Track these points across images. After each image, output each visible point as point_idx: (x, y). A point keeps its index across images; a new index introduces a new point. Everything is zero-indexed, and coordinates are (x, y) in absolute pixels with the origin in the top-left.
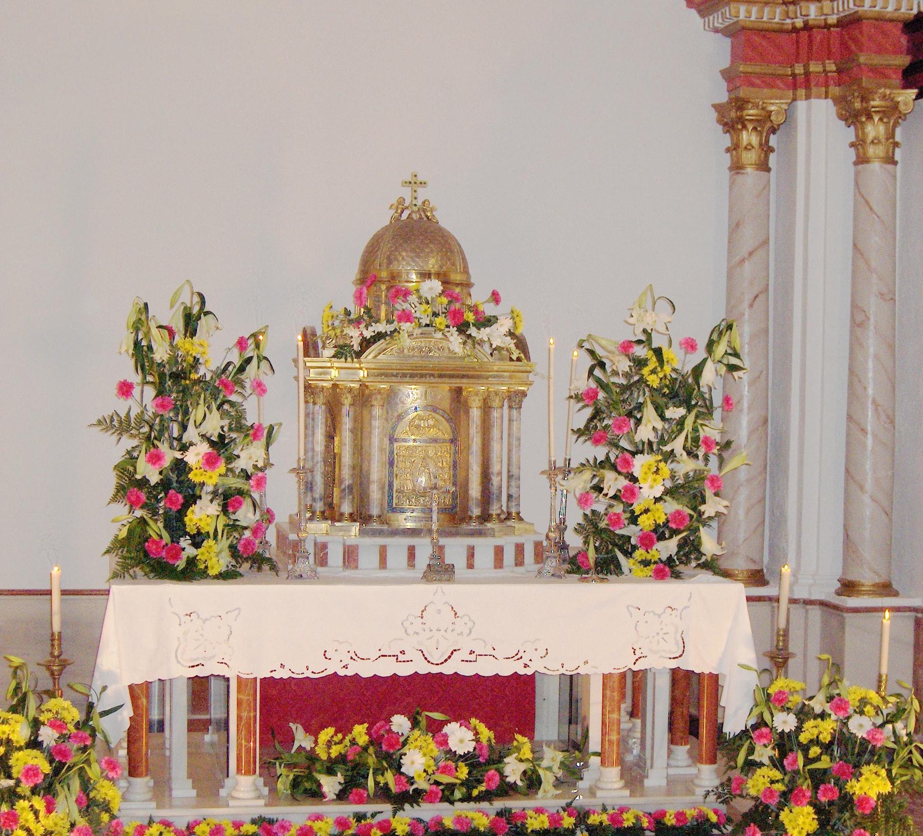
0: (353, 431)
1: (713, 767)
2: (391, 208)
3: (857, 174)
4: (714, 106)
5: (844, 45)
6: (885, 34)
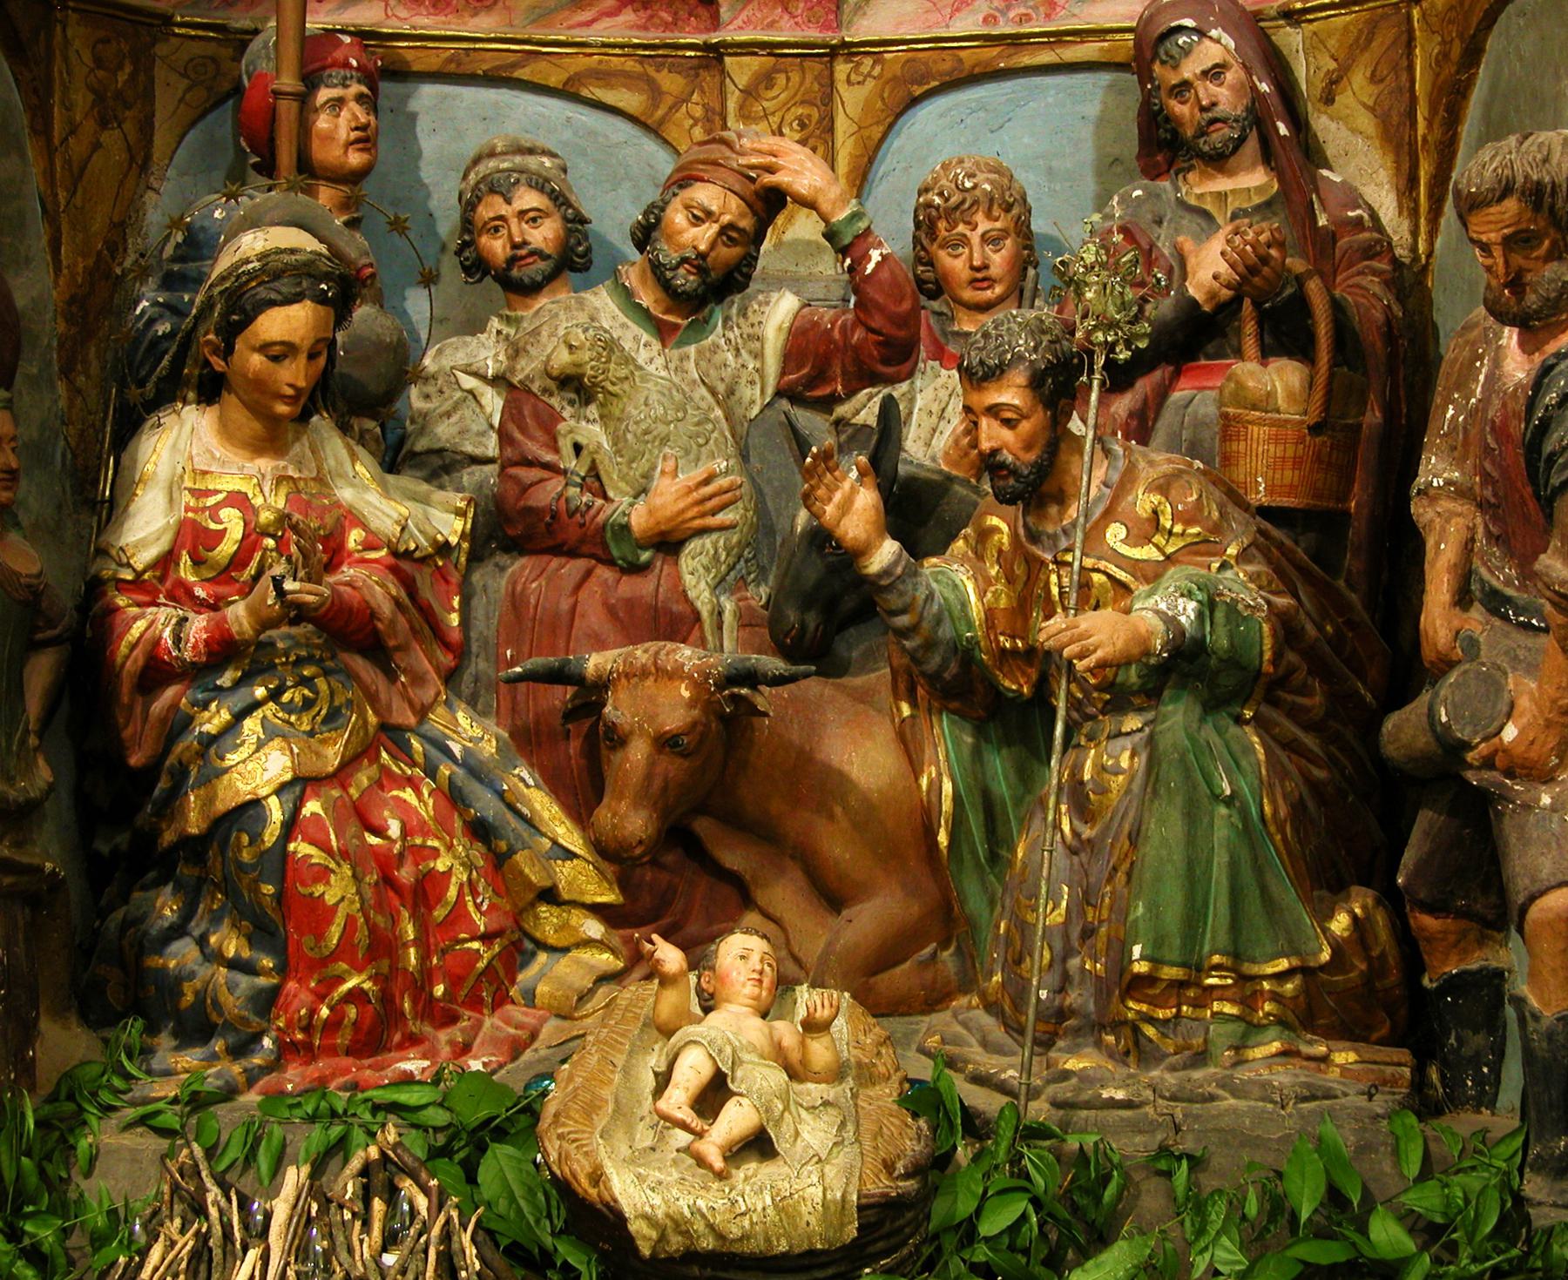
2: (92, 1160)
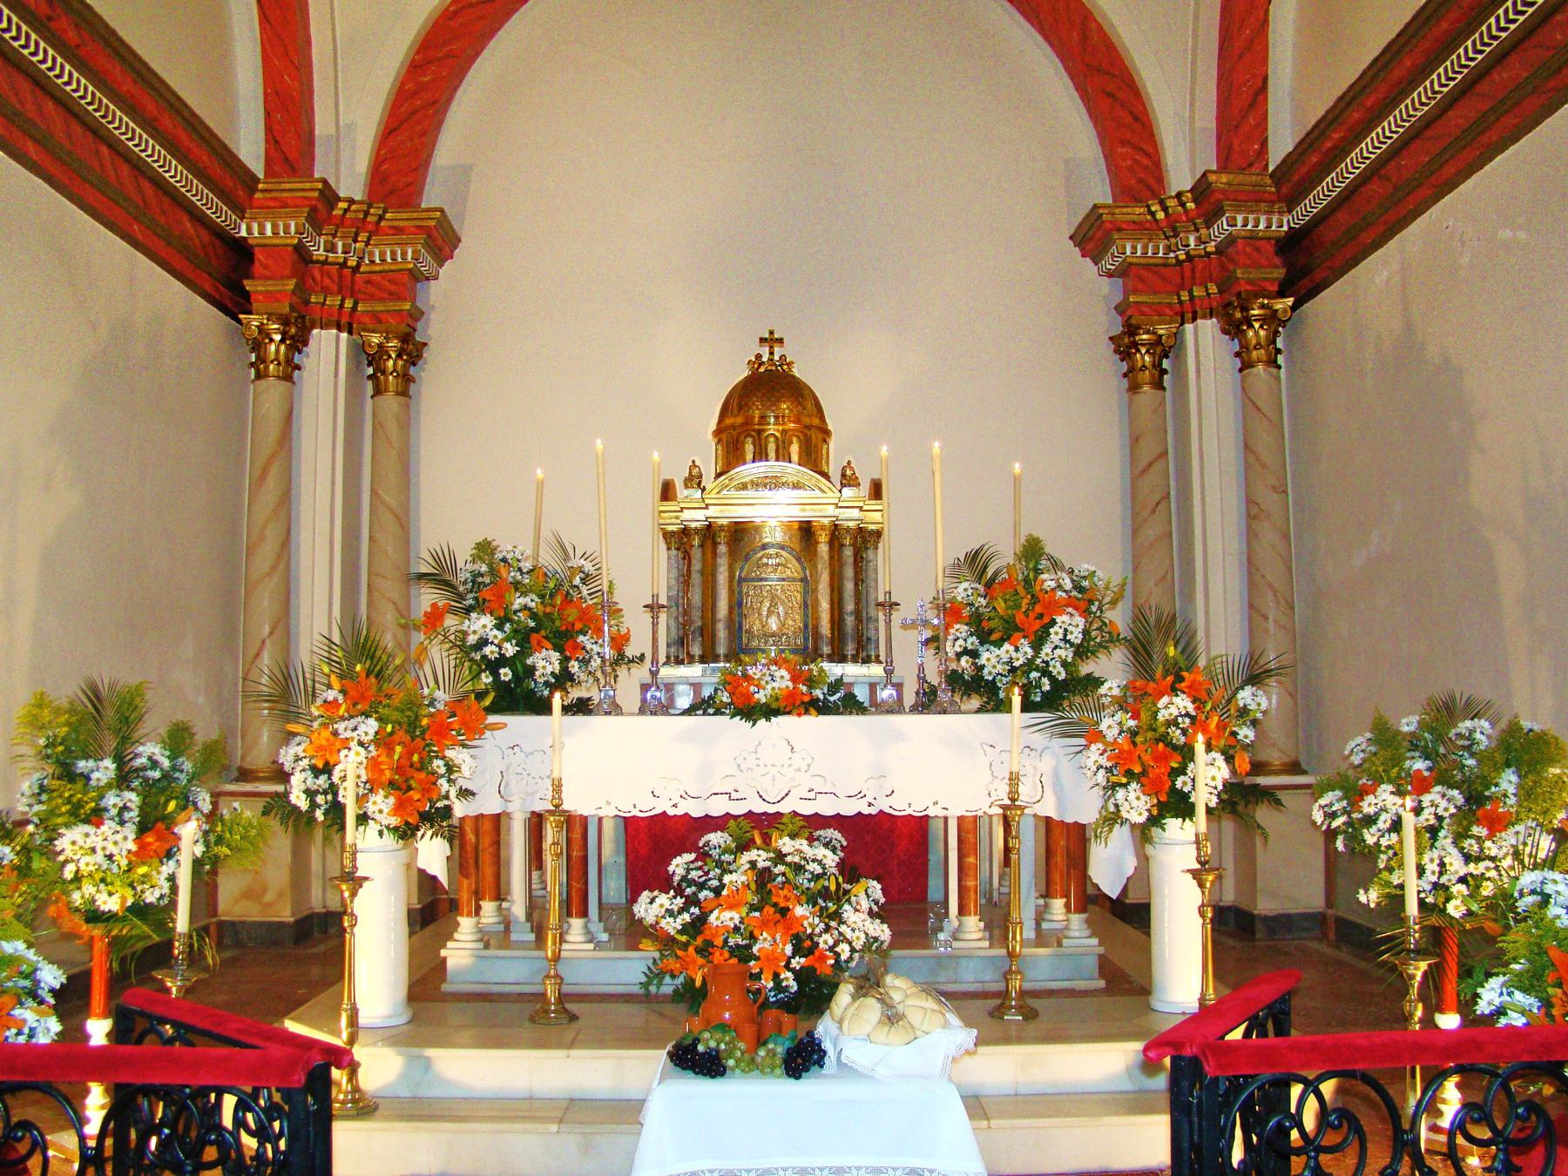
0: (702, 572)
1: (1084, 916)
3: (1243, 381)
4: (1111, 339)
5: (1223, 268)
6: (1258, 250)
